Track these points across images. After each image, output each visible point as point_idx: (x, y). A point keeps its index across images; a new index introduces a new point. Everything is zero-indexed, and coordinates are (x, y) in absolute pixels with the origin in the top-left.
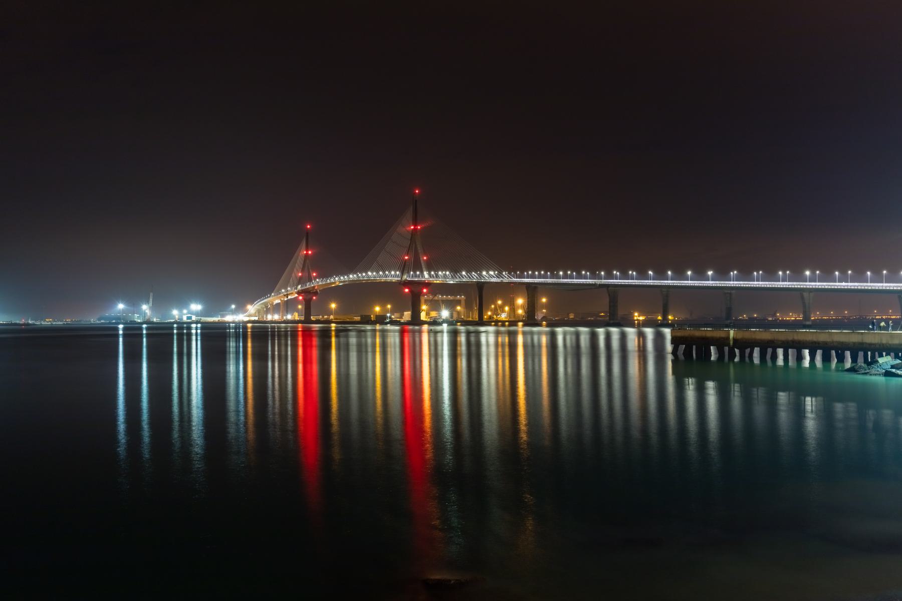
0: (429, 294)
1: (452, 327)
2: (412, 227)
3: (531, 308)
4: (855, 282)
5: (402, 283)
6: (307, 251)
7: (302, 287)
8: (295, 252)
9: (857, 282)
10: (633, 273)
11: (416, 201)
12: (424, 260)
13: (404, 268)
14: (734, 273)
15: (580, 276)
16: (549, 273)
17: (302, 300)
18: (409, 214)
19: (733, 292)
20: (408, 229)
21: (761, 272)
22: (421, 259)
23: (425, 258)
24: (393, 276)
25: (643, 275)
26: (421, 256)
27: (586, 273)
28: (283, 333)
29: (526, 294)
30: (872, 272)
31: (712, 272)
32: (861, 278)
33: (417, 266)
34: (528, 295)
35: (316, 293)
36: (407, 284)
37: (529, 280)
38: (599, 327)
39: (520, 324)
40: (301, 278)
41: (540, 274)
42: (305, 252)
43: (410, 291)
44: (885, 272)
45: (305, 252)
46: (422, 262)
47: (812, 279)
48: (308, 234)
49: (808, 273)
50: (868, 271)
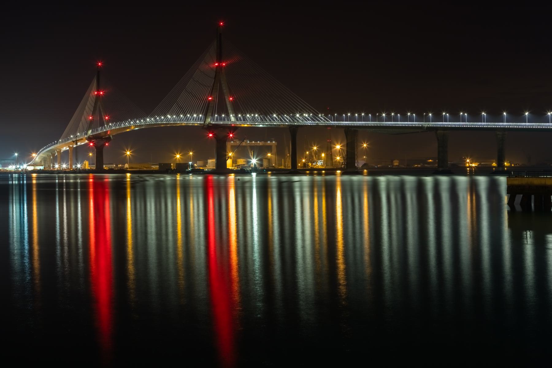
5: (205, 127)
6: (98, 91)
7: (92, 132)
13: (207, 111)
15: (405, 119)
20: (212, 66)
22: (227, 100)
26: (226, 97)
27: (198, 115)
33: (222, 109)
40: (91, 121)
46: (228, 103)
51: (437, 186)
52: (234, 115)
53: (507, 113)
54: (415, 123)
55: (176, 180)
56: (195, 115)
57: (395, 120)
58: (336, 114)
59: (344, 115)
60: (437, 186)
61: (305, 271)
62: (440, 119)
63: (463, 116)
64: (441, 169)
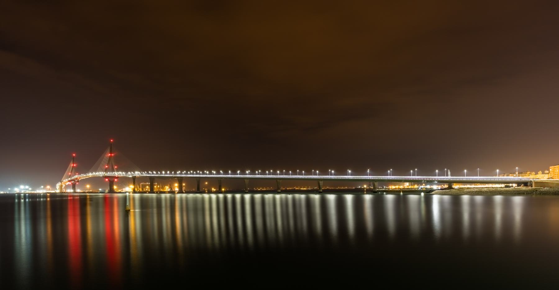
0: (61, 180)
1: (16, 197)
2: (110, 155)
3: (180, 187)
4: (327, 175)
6: (73, 164)
8: (69, 165)
9: (263, 175)
10: (200, 172)
11: (111, 144)
12: (115, 168)
13: (106, 170)
14: (390, 171)
15: (204, 173)
16: (303, 172)
17: (107, 181)
18: (108, 150)
19: (278, 181)
20: (108, 155)
21: (391, 170)
23: (116, 167)
24: (101, 174)
25: (234, 172)
27: (200, 172)
28: (22, 195)
29: (178, 181)
30: (439, 170)
31: (239, 171)
32: (287, 174)
33: (113, 170)
34: (179, 181)
35: (78, 181)
36: (106, 177)
37: (191, 175)
38: (348, 194)
39: (131, 193)
40: (70, 175)
41: (258, 172)
42: (72, 165)
43: (109, 180)
44: (416, 169)
45: (72, 165)
47: (414, 175)
48: (74, 157)
49: (257, 172)
50: (169, 171)
51: (253, 200)
52: (77, 174)
53: (291, 172)
54: (369, 177)
55: (175, 198)
56: (198, 172)
57: (199, 174)
58: (446, 169)
59: (412, 171)
60: (243, 200)
61: (75, 215)
62: (219, 174)
63: (206, 173)
64: (198, 192)
